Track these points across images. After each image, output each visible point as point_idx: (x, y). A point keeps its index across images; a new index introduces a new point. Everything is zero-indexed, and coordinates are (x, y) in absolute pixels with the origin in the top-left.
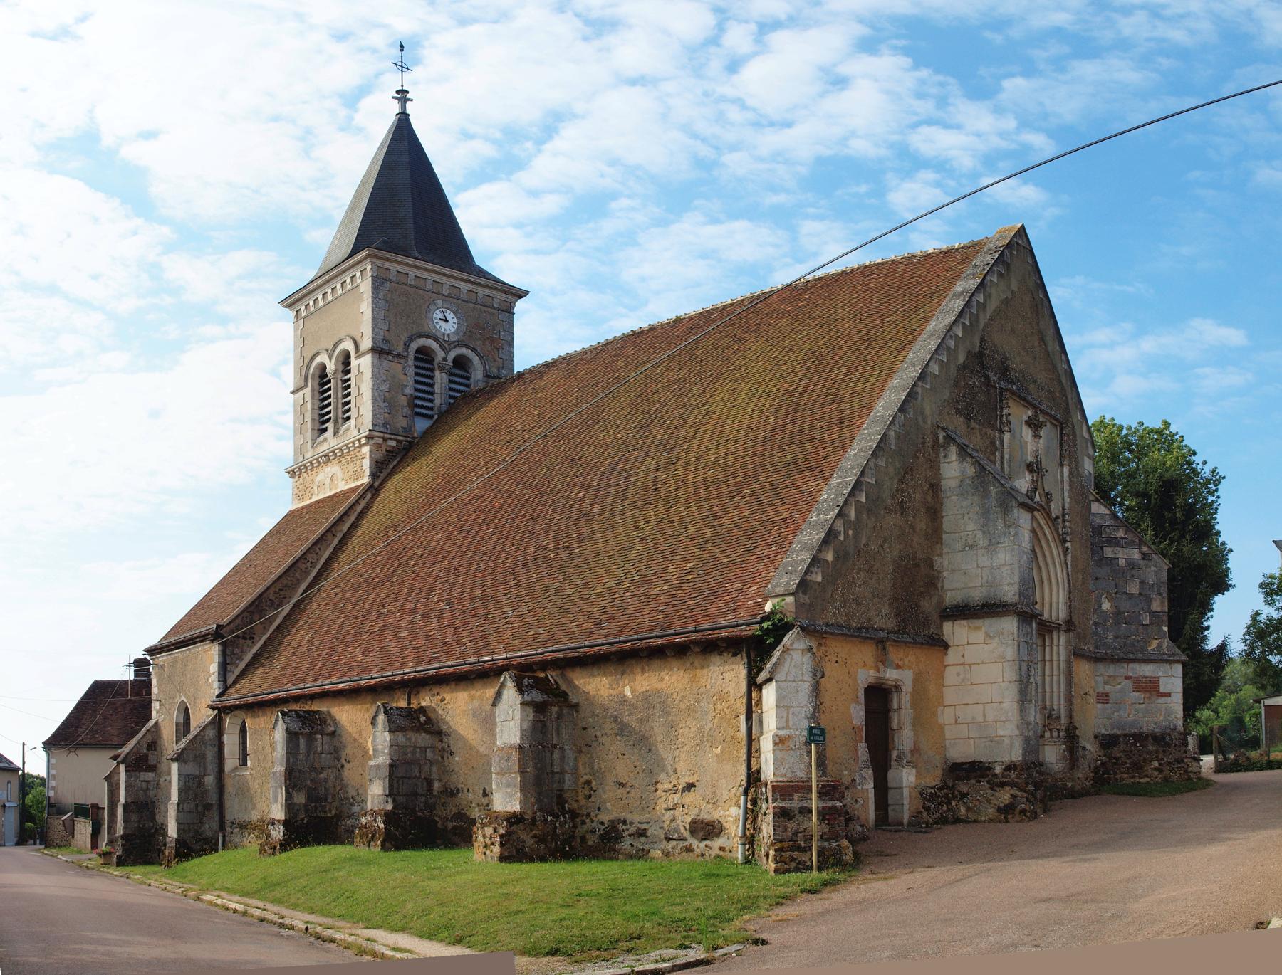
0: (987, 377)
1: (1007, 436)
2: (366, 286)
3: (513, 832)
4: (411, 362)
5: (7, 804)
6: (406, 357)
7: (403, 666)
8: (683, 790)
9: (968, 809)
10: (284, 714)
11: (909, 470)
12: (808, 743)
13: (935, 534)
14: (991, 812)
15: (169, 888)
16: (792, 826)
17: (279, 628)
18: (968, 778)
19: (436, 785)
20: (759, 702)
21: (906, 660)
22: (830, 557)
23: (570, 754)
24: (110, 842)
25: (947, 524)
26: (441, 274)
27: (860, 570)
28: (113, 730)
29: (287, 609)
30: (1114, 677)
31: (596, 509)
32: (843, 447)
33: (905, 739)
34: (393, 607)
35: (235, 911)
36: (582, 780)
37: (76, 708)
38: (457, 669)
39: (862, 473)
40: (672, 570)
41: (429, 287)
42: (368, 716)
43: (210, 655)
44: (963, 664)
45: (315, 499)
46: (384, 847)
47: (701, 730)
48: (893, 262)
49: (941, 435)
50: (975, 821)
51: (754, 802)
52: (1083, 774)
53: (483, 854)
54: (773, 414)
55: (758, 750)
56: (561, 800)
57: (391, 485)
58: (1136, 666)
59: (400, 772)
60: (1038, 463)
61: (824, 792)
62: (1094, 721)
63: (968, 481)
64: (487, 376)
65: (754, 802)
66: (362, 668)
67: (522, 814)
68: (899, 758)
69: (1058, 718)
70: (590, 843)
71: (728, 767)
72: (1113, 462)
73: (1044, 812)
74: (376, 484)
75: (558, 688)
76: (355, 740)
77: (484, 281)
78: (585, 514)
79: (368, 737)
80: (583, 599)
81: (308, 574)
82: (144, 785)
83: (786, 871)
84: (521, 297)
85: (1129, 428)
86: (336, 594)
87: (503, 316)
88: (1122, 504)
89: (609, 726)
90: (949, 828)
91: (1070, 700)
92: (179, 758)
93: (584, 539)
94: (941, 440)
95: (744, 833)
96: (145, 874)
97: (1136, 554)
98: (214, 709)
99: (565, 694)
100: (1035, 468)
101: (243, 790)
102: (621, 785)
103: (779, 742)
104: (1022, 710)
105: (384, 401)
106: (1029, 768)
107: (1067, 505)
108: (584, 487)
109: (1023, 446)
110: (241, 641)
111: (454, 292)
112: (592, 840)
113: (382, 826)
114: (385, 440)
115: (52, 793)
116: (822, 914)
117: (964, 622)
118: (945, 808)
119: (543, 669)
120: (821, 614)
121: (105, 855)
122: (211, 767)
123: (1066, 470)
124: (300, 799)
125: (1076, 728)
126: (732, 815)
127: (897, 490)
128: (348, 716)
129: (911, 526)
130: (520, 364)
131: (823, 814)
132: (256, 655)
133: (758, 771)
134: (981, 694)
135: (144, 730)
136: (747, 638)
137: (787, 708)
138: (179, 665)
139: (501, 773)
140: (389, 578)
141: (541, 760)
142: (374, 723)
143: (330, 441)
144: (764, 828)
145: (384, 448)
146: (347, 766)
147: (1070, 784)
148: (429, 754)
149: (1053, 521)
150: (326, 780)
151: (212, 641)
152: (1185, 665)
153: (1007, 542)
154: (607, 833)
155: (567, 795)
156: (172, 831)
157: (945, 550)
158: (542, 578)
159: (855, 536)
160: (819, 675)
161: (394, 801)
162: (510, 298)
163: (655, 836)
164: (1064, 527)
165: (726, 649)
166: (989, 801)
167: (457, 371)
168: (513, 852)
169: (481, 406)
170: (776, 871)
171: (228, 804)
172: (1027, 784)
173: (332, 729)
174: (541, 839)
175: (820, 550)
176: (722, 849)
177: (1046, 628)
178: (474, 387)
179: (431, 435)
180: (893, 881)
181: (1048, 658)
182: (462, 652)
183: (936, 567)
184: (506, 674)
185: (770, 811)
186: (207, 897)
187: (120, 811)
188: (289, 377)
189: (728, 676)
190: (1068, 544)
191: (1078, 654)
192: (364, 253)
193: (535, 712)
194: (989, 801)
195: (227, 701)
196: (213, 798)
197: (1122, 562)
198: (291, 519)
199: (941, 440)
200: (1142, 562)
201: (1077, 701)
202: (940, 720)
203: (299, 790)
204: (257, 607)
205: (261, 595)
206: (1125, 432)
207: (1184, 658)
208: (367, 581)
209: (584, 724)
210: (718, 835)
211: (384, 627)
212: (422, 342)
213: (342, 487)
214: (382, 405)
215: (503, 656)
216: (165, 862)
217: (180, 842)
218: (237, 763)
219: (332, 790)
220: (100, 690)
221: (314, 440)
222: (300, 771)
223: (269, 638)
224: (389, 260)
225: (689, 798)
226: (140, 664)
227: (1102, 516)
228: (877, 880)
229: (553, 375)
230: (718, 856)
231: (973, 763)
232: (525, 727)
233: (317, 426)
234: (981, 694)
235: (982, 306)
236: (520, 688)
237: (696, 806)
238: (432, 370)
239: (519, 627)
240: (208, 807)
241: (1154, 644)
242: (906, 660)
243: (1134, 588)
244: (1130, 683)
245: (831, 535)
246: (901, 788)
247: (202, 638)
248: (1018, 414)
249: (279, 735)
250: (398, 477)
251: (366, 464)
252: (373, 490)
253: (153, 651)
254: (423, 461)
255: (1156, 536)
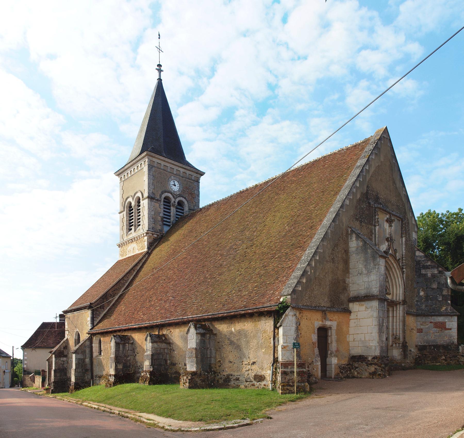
0: (369, 203)
1: (377, 228)
2: (146, 169)
3: (193, 378)
4: (162, 203)
5: (6, 371)
6: (160, 201)
7: (157, 319)
8: (252, 364)
9: (358, 373)
10: (114, 336)
11: (336, 245)
12: (293, 348)
13: (346, 270)
14: (367, 374)
15: (71, 401)
16: (288, 377)
17: (113, 305)
18: (358, 361)
19: (169, 362)
20: (278, 334)
21: (334, 318)
22: (304, 281)
23: (213, 352)
24: (49, 384)
25: (351, 265)
26: (173, 164)
27: (316, 285)
28: (51, 341)
29: (117, 297)
30: (425, 322)
31: (225, 263)
32: (311, 238)
33: (333, 346)
34: (154, 298)
35: (95, 408)
36: (217, 360)
37: (35, 333)
38: (175, 321)
39: (317, 248)
40: (249, 286)
41: (169, 170)
42: (145, 337)
43: (88, 314)
44: (357, 319)
45: (127, 256)
46: (149, 384)
47: (258, 343)
48: (335, 154)
49: (349, 230)
50: (361, 378)
51: (276, 369)
52: (409, 361)
53: (183, 385)
54: (287, 225)
55: (277, 350)
56: (210, 367)
57: (155, 252)
58: (435, 317)
59: (155, 357)
60: (391, 238)
61: (299, 366)
62: (415, 340)
63: (360, 248)
64: (189, 209)
65: (276, 369)
66: (143, 320)
67: (196, 372)
68: (331, 354)
69: (399, 339)
70: (220, 382)
71: (267, 356)
72: (434, 231)
73: (389, 375)
74: (150, 252)
75: (209, 328)
76: (140, 346)
77: (189, 168)
78: (221, 265)
79: (144, 344)
80: (219, 297)
81: (124, 285)
82: (62, 362)
83: (285, 394)
84: (202, 175)
85: (442, 214)
86: (134, 293)
87: (196, 184)
88: (438, 248)
89: (227, 342)
90: (350, 380)
91: (404, 331)
92: (76, 352)
93: (220, 275)
94: (349, 232)
95: (272, 380)
96: (62, 396)
97: (436, 271)
98: (89, 334)
99: (212, 330)
100: (390, 240)
101: (100, 364)
102: (231, 362)
103: (284, 348)
104: (380, 336)
105: (152, 219)
106: (382, 358)
107: (404, 254)
108: (221, 255)
109: (385, 230)
110: (99, 309)
111: (178, 172)
112: (221, 381)
113: (149, 376)
114: (153, 234)
115: (25, 366)
116: (294, 409)
117: (357, 303)
118: (349, 372)
119: (204, 322)
120: (301, 302)
121: (47, 389)
122: (88, 356)
123: (404, 239)
124: (120, 367)
125: (406, 343)
126: (268, 373)
127: (331, 254)
128: (138, 337)
129: (337, 267)
130: (202, 205)
131: (299, 374)
132: (105, 314)
133: (277, 358)
134: (363, 329)
135: (62, 342)
136: (274, 311)
137: (287, 336)
138: (76, 318)
139: (190, 358)
140: (153, 288)
141: (202, 354)
142: (146, 340)
143: (133, 234)
144: (278, 378)
145: (152, 238)
146: (137, 355)
147: (403, 365)
148: (166, 351)
149: (397, 261)
150: (130, 360)
151: (88, 309)
152: (458, 316)
153: (374, 271)
154: (226, 379)
155: (212, 365)
156: (73, 379)
157: (350, 276)
158: (206, 289)
159: (314, 272)
160: (298, 324)
161: (153, 367)
162: (198, 176)
163: (242, 380)
164: (402, 263)
165: (267, 315)
166: (366, 370)
167: (179, 207)
168: (193, 385)
169: (187, 222)
170: (282, 393)
171: (94, 369)
172: (381, 364)
173: (132, 342)
174: (203, 381)
175: (300, 278)
176: (265, 385)
177: (393, 304)
178: (185, 214)
179: (170, 233)
180: (323, 399)
181: (395, 315)
182: (177, 315)
183: (347, 282)
184: (191, 323)
185: (280, 372)
186: (85, 404)
187: (53, 373)
188: (118, 207)
189: (267, 324)
190: (404, 270)
191: (408, 314)
192: (145, 153)
193: (201, 336)
194: (366, 370)
195: (94, 331)
196: (89, 367)
197: (429, 275)
198: (119, 263)
199: (349, 232)
200: (439, 275)
201: (408, 332)
202: (348, 340)
203: (120, 364)
204: (105, 297)
205: (107, 292)
206: (440, 216)
207: (458, 314)
208: (146, 288)
209: (218, 341)
210: (263, 380)
211: (151, 305)
212: (166, 194)
213: (137, 252)
214: (152, 220)
215: (191, 317)
216: (70, 391)
217: (75, 383)
218: (98, 354)
219: (132, 364)
220: (45, 326)
221: (127, 233)
222: (120, 357)
223: (110, 308)
224: (154, 157)
225: (254, 367)
226: (61, 316)
227: (421, 257)
228: (317, 398)
229: (212, 210)
230: (263, 388)
231: (360, 356)
232: (198, 341)
233: (128, 227)
234: (363, 329)
235: (368, 171)
236: (196, 328)
237: (256, 370)
238: (170, 206)
239: (197, 306)
240: (87, 370)
241: (444, 308)
242: (334, 318)
243: (435, 286)
244: (432, 324)
245: (305, 272)
246: (331, 364)
247: (84, 308)
248: (382, 217)
249: (113, 344)
250: (157, 249)
251: (146, 243)
252: (148, 254)
253: (66, 312)
254: (166, 243)
255: (453, 261)
